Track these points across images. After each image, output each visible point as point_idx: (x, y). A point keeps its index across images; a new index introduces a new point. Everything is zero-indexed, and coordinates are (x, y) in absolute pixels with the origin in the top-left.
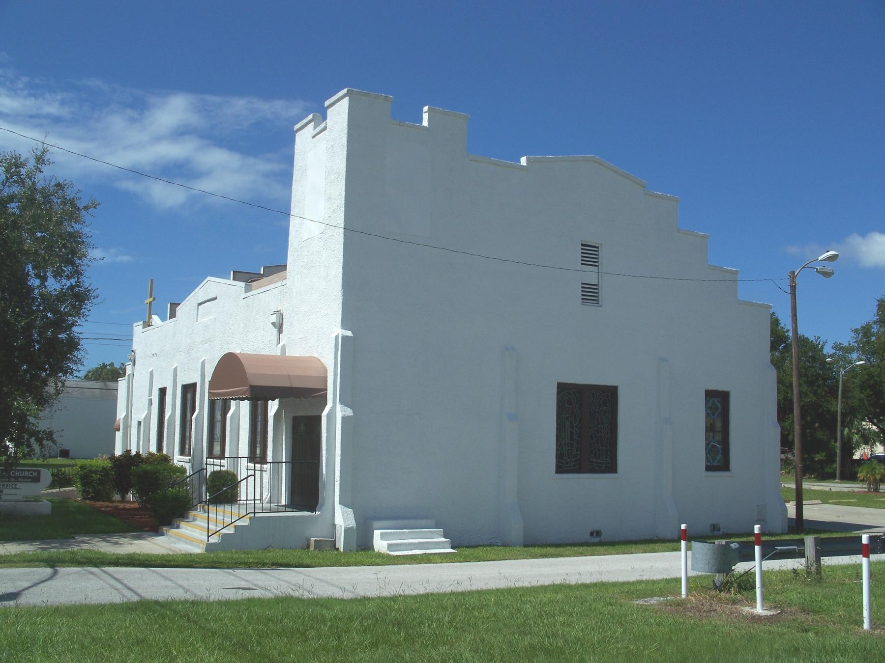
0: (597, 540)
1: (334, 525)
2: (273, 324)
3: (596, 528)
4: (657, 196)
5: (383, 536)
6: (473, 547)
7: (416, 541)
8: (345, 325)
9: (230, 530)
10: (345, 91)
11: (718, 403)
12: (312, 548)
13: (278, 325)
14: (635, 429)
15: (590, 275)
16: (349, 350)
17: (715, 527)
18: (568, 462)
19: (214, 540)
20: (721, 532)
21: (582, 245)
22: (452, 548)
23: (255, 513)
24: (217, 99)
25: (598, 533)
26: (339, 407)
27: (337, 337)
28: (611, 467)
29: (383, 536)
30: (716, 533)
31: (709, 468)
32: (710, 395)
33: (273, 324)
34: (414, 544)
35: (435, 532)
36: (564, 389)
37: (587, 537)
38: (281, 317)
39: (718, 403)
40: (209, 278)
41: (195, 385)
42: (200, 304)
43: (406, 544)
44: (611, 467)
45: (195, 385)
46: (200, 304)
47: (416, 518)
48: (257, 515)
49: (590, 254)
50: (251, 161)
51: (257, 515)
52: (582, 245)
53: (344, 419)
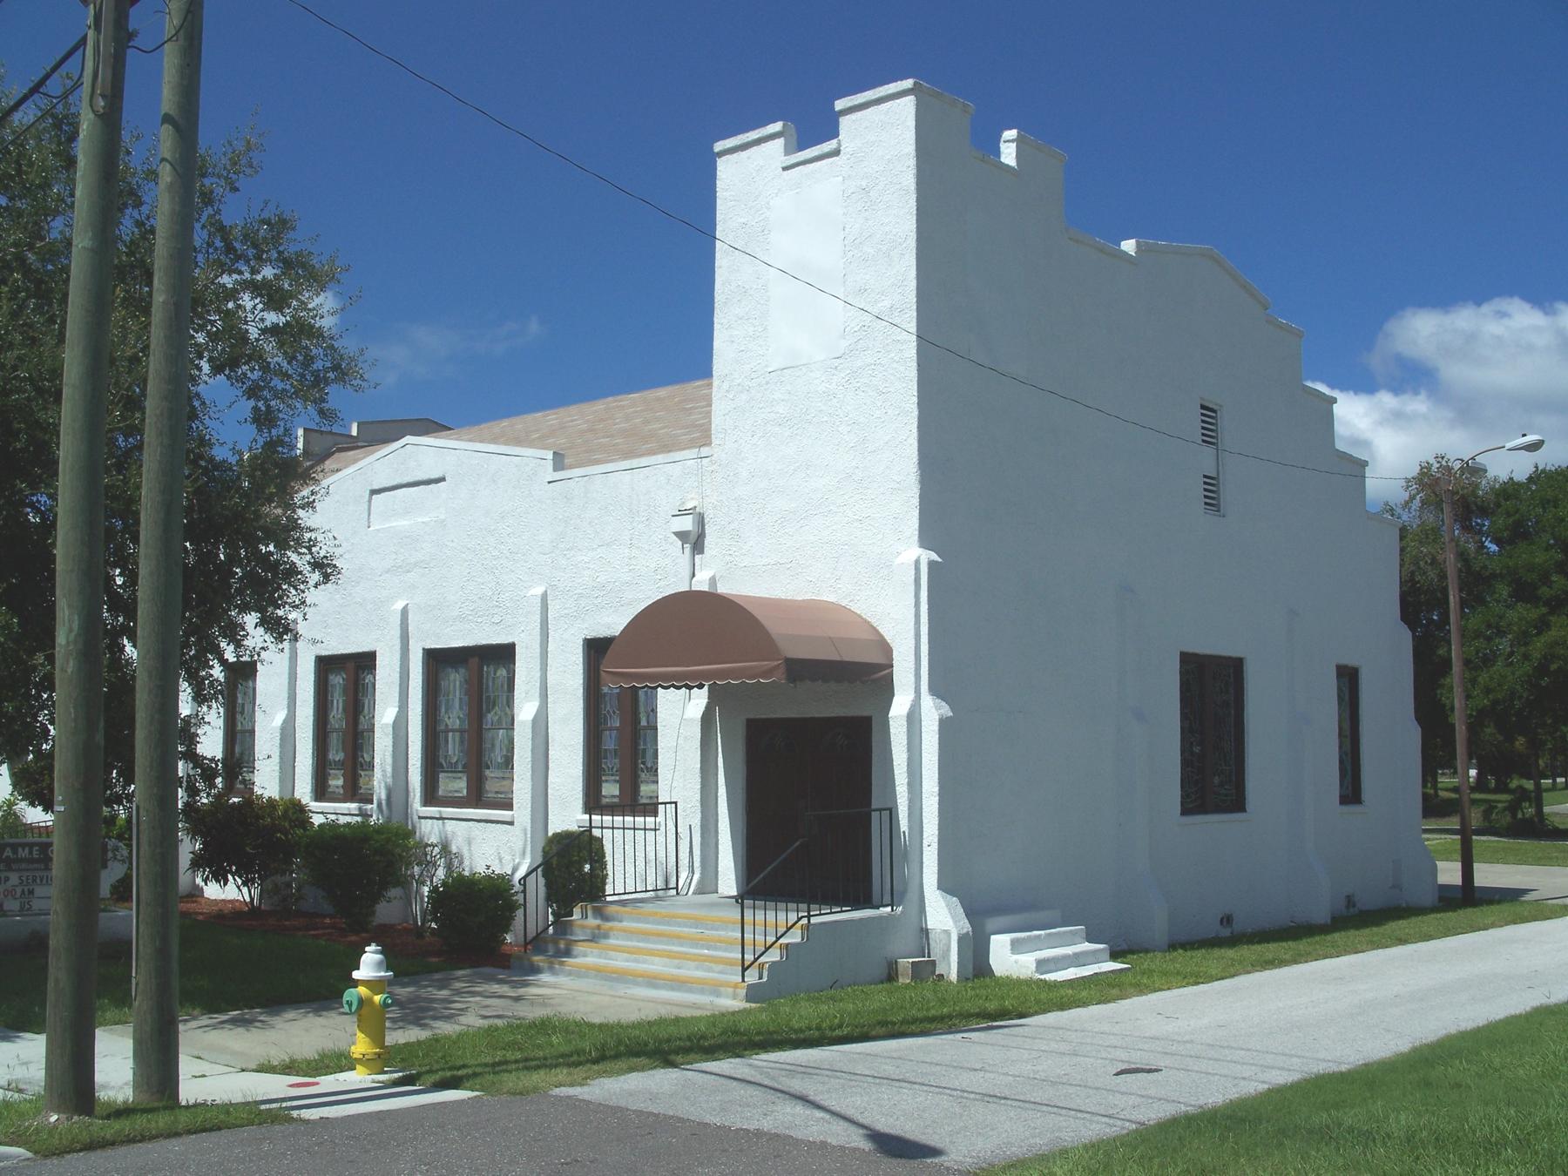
1: (925, 932)
2: (682, 536)
4: (1280, 326)
5: (1016, 947)
7: (1069, 950)
8: (926, 540)
9: (774, 956)
10: (908, 83)
11: (1349, 678)
12: (904, 980)
13: (693, 538)
16: (947, 594)
18: (1344, 800)
19: (752, 977)
21: (1203, 407)
22: (1114, 956)
23: (809, 917)
26: (928, 702)
27: (917, 562)
29: (1016, 947)
33: (682, 536)
36: (1186, 658)
38: (701, 521)
39: (1349, 678)
40: (408, 439)
41: (504, 654)
42: (374, 492)
45: (504, 654)
46: (374, 492)
48: (813, 920)
51: (813, 920)
52: (1203, 407)
53: (943, 723)
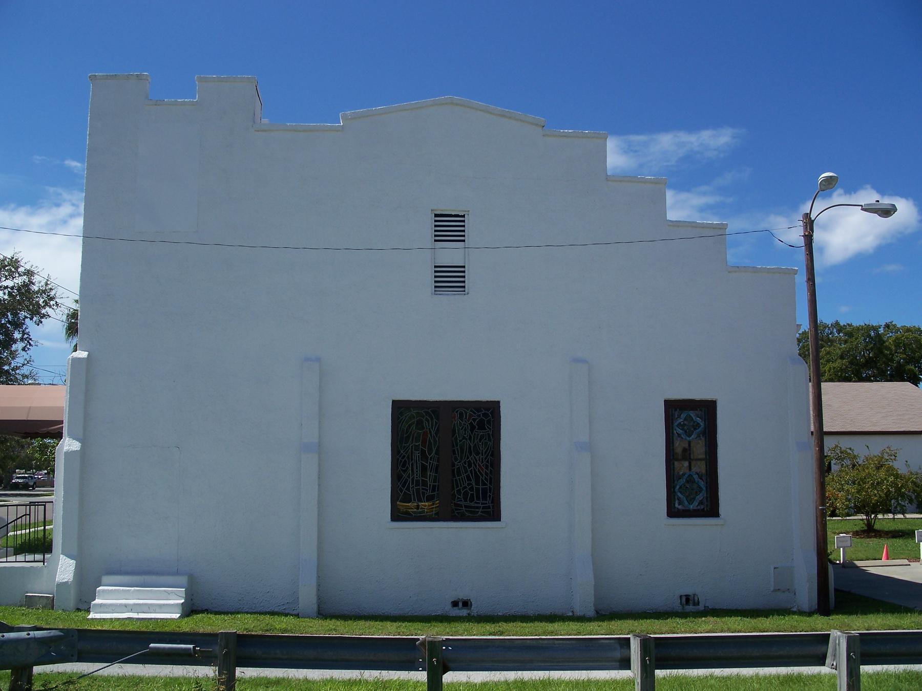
0: (464, 612)
3: (462, 595)
6: (232, 613)
14: (524, 461)
15: (450, 254)
17: (687, 599)
20: (701, 607)
24: (642, 138)
25: (466, 604)
28: (492, 513)
30: (690, 608)
31: (673, 513)
32: (673, 408)
34: (126, 606)
35: (172, 592)
36: (400, 409)
37: (676, 605)
43: (121, 605)
44: (492, 513)
47: (157, 574)
49: (449, 227)
50: (684, 196)
52: (436, 215)
